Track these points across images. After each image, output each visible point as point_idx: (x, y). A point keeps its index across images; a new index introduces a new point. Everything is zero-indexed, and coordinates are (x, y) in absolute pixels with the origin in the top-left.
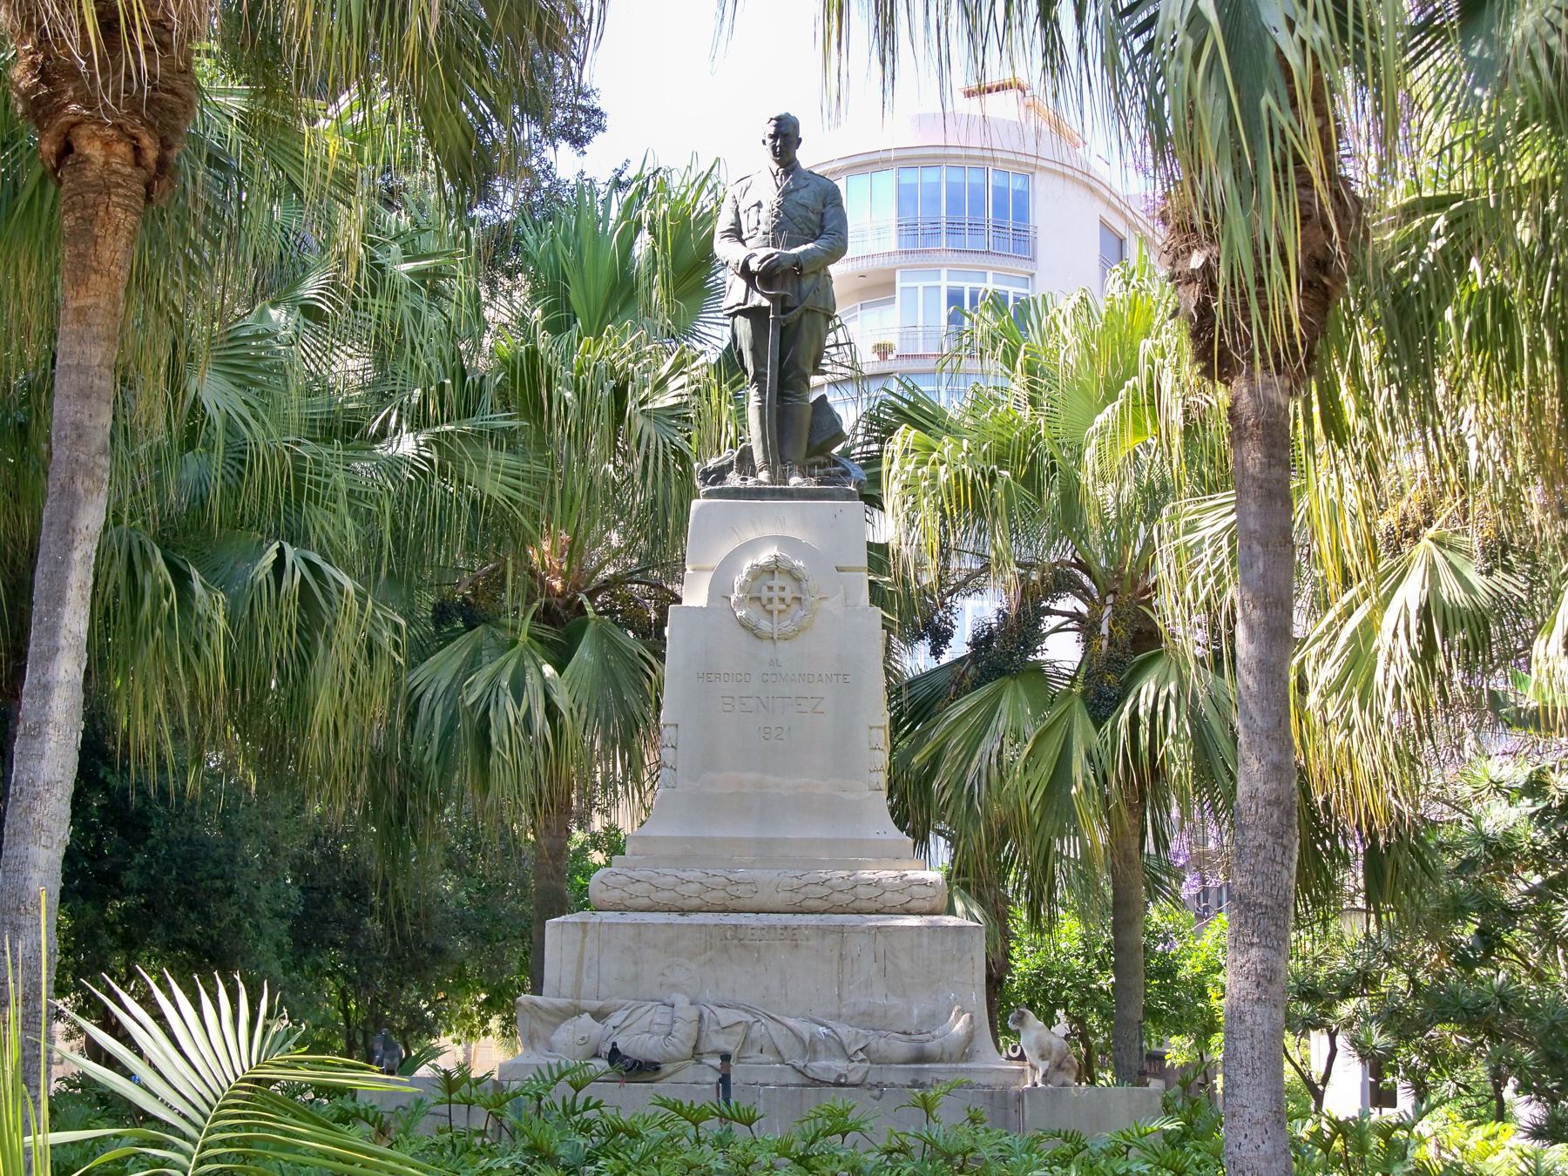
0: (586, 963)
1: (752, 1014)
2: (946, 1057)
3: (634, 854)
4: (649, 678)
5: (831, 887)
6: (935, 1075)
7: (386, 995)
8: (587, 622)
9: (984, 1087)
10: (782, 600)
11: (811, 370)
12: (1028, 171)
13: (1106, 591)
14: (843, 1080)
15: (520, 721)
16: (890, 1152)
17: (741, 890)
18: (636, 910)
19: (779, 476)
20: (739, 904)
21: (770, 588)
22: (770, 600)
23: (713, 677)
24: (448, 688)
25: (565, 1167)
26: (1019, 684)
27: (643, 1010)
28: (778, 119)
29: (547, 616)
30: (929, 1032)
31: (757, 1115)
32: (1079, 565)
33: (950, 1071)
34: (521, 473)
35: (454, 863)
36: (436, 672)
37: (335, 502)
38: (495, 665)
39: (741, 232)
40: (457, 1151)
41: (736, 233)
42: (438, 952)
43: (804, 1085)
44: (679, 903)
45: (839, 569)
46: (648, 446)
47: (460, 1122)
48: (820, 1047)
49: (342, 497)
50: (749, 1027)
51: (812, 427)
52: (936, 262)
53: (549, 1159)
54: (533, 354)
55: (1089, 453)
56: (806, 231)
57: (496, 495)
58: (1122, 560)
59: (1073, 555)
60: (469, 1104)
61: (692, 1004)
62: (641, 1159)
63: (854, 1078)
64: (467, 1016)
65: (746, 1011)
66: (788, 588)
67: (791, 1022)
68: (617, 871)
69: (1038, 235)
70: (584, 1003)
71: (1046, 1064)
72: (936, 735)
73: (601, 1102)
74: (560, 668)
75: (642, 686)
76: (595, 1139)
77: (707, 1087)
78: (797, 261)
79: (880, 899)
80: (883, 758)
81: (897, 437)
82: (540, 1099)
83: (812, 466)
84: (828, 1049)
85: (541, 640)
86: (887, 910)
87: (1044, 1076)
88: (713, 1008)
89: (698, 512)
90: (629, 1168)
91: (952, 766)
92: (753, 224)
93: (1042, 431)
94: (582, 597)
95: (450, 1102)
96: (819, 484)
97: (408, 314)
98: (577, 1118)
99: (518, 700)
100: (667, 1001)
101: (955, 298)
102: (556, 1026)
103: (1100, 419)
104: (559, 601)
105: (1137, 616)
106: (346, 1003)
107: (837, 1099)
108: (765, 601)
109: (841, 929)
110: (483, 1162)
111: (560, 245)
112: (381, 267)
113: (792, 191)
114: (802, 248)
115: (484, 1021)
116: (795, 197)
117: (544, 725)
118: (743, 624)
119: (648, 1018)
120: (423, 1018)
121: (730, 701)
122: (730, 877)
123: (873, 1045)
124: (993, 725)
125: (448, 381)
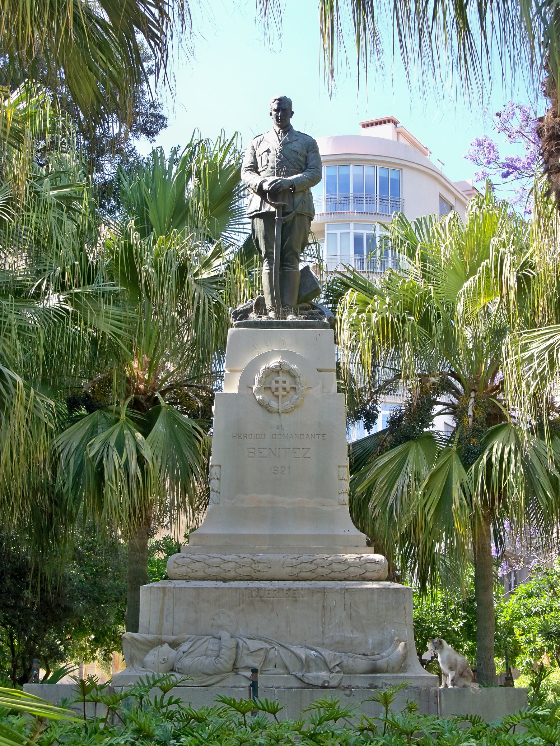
0: (165, 612)
1: (270, 643)
2: (390, 669)
3: (194, 545)
4: (199, 441)
5: (316, 565)
6: (384, 681)
7: (36, 636)
8: (160, 408)
9: (414, 688)
10: (284, 389)
11: (300, 251)
12: (399, 170)
13: (468, 390)
14: (326, 685)
15: (122, 466)
16: (362, 730)
17: (261, 567)
18: (196, 579)
19: (279, 314)
20: (258, 575)
21: (277, 382)
22: (277, 389)
23: (242, 436)
24: (78, 447)
25: (158, 742)
26: (419, 446)
27: (201, 641)
28: (280, 100)
29: (136, 405)
30: (379, 654)
31: (279, 707)
32: (453, 374)
33: (394, 678)
34: (122, 318)
35: (79, 557)
36: (70, 438)
37: (10, 332)
38: (106, 433)
39: (257, 168)
40: (89, 732)
41: (254, 168)
42: (68, 610)
43: (302, 688)
44: (223, 575)
45: (319, 370)
46: (198, 303)
47: (90, 714)
48: (312, 664)
49: (14, 331)
50: (267, 651)
51: (300, 285)
52: (347, 219)
53: (149, 737)
54: (129, 248)
55: (460, 307)
56: (297, 167)
57: (107, 331)
58: (479, 369)
59: (450, 369)
60: (96, 701)
61: (232, 637)
62: (209, 736)
63: (334, 683)
64: (83, 649)
65: (266, 642)
66: (288, 382)
67: (293, 649)
68: (184, 555)
69: (405, 204)
70: (164, 637)
71: (454, 672)
72: (370, 475)
73: (179, 699)
74: (145, 435)
75: (195, 446)
76: (176, 723)
77: (242, 689)
78: (292, 184)
79: (346, 571)
80: (346, 486)
81: (347, 297)
82: (141, 698)
83: (301, 309)
84: (317, 665)
85: (132, 419)
86: (351, 578)
87: (452, 680)
88: (245, 639)
89: (232, 336)
90: (202, 743)
91: (379, 494)
92: (265, 163)
93: (432, 294)
94: (157, 394)
95: (84, 701)
96: (306, 319)
97: (54, 221)
98: (164, 710)
99: (121, 454)
100: (216, 635)
101: (358, 240)
102: (147, 652)
103: (466, 285)
104: (143, 397)
105: (489, 404)
106: (12, 641)
107: (327, 697)
108: (273, 389)
109: (323, 590)
110: (106, 740)
111: (144, 186)
112: (37, 193)
113: (288, 143)
114: (295, 176)
115: (93, 651)
116: (290, 146)
117: (136, 468)
118: (260, 403)
119: (204, 646)
120: (58, 651)
121: (252, 450)
122: (254, 558)
123: (345, 662)
124: (404, 469)
125: (77, 263)
